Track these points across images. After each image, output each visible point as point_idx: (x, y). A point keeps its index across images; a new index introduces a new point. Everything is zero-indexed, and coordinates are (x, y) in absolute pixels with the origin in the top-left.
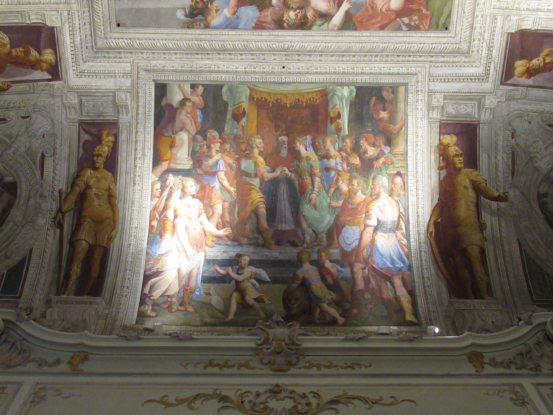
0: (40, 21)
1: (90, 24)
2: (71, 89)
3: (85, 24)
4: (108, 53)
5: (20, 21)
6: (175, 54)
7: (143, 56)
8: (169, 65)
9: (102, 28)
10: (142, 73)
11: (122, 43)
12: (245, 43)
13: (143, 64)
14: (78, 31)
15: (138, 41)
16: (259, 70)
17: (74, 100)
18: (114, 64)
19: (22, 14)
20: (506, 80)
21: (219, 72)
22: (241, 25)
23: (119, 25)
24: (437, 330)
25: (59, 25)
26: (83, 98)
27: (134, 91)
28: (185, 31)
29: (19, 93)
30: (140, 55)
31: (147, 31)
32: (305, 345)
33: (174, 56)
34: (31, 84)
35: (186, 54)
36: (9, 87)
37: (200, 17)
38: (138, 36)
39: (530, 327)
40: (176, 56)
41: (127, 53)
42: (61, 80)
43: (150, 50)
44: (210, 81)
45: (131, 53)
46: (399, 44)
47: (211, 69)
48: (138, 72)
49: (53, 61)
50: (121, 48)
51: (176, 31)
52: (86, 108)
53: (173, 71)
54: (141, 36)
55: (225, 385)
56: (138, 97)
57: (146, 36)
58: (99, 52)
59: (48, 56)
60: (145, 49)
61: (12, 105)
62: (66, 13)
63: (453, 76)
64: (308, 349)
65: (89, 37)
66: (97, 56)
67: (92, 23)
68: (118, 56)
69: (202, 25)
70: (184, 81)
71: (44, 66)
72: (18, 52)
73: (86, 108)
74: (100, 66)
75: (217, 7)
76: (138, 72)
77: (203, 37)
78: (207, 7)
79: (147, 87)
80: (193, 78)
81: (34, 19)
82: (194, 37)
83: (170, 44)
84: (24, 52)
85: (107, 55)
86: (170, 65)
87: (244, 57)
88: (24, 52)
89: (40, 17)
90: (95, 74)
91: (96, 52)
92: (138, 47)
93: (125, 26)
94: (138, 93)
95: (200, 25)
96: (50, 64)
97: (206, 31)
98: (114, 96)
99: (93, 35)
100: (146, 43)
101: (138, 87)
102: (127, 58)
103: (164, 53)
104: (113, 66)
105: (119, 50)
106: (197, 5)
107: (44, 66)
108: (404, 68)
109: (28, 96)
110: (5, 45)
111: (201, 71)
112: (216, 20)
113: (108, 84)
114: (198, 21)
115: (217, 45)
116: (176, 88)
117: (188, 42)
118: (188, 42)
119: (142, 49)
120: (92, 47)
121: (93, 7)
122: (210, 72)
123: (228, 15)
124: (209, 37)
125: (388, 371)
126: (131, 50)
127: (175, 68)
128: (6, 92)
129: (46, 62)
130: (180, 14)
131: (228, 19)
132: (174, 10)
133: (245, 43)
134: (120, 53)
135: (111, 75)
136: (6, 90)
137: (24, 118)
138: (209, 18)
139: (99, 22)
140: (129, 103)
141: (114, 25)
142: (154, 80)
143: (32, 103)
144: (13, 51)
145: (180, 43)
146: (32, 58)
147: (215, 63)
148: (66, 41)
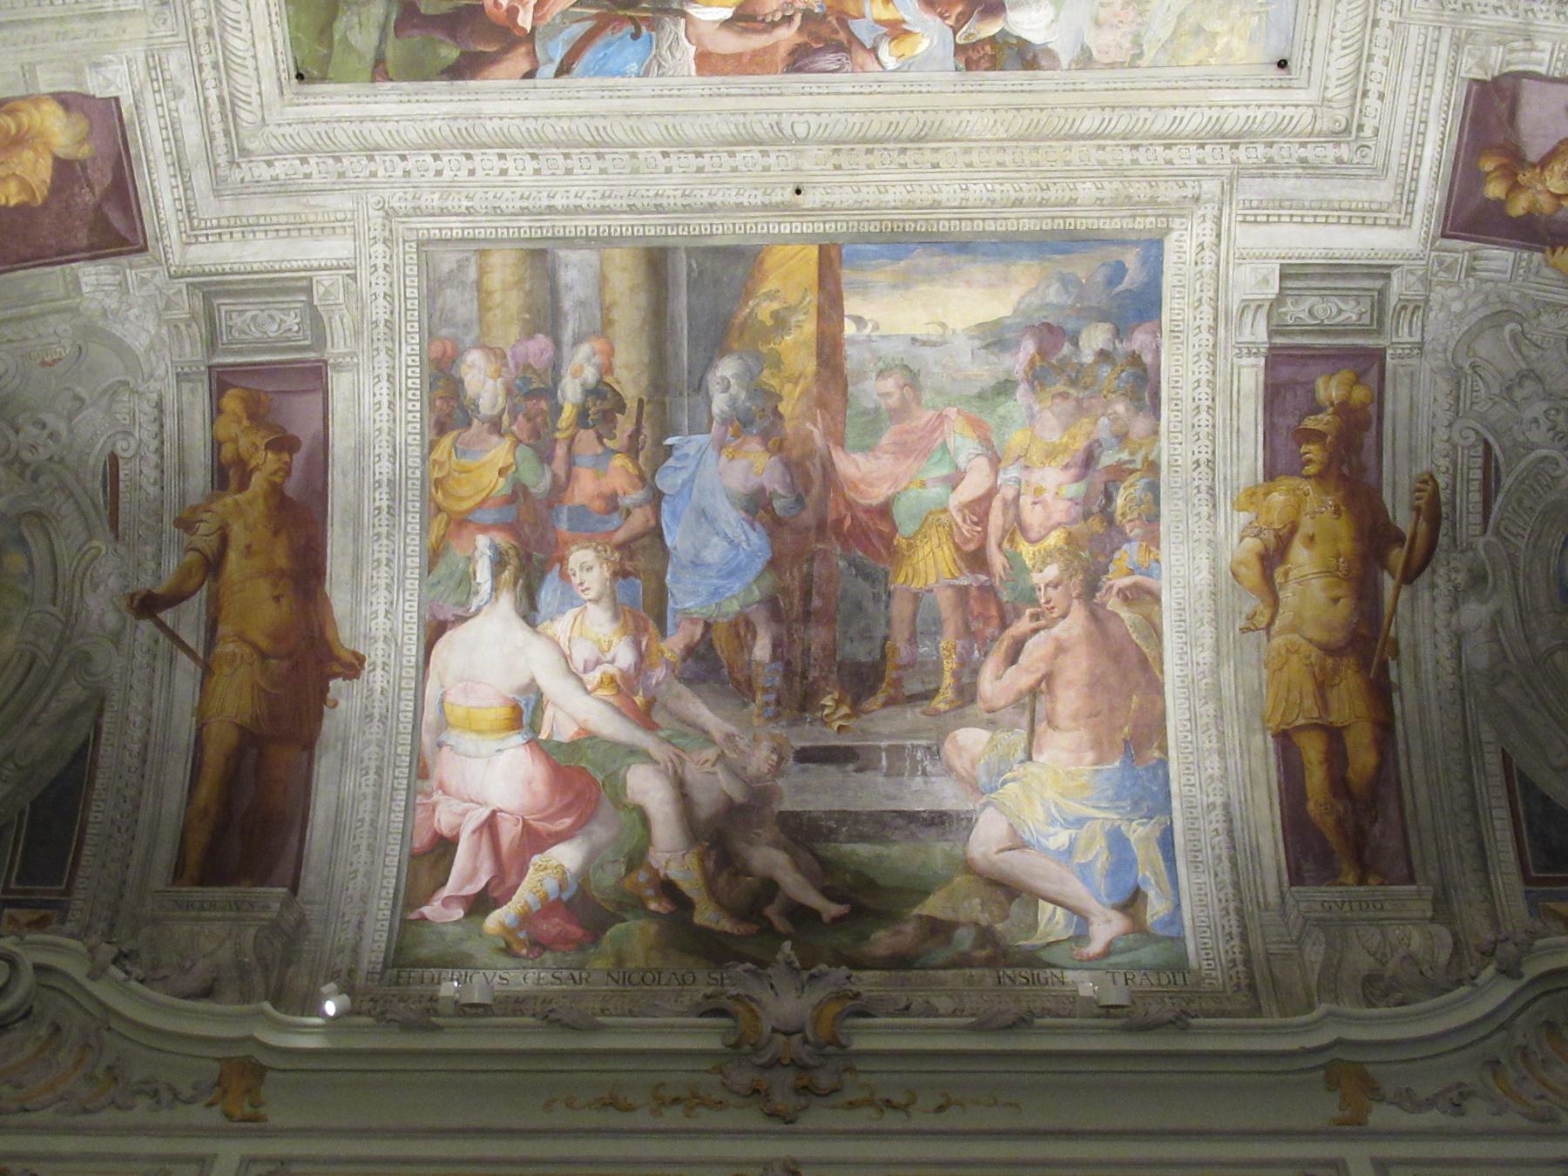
16: (565, 202)
20: (124, 241)
24: (330, 1008)
32: (860, 1043)
39: (1518, 984)
43: (591, 146)
46: (835, 116)
63: (1281, 207)
64: (861, 1054)
92: (588, 138)
93: (313, 80)
108: (1007, 186)
125: (1118, 1123)
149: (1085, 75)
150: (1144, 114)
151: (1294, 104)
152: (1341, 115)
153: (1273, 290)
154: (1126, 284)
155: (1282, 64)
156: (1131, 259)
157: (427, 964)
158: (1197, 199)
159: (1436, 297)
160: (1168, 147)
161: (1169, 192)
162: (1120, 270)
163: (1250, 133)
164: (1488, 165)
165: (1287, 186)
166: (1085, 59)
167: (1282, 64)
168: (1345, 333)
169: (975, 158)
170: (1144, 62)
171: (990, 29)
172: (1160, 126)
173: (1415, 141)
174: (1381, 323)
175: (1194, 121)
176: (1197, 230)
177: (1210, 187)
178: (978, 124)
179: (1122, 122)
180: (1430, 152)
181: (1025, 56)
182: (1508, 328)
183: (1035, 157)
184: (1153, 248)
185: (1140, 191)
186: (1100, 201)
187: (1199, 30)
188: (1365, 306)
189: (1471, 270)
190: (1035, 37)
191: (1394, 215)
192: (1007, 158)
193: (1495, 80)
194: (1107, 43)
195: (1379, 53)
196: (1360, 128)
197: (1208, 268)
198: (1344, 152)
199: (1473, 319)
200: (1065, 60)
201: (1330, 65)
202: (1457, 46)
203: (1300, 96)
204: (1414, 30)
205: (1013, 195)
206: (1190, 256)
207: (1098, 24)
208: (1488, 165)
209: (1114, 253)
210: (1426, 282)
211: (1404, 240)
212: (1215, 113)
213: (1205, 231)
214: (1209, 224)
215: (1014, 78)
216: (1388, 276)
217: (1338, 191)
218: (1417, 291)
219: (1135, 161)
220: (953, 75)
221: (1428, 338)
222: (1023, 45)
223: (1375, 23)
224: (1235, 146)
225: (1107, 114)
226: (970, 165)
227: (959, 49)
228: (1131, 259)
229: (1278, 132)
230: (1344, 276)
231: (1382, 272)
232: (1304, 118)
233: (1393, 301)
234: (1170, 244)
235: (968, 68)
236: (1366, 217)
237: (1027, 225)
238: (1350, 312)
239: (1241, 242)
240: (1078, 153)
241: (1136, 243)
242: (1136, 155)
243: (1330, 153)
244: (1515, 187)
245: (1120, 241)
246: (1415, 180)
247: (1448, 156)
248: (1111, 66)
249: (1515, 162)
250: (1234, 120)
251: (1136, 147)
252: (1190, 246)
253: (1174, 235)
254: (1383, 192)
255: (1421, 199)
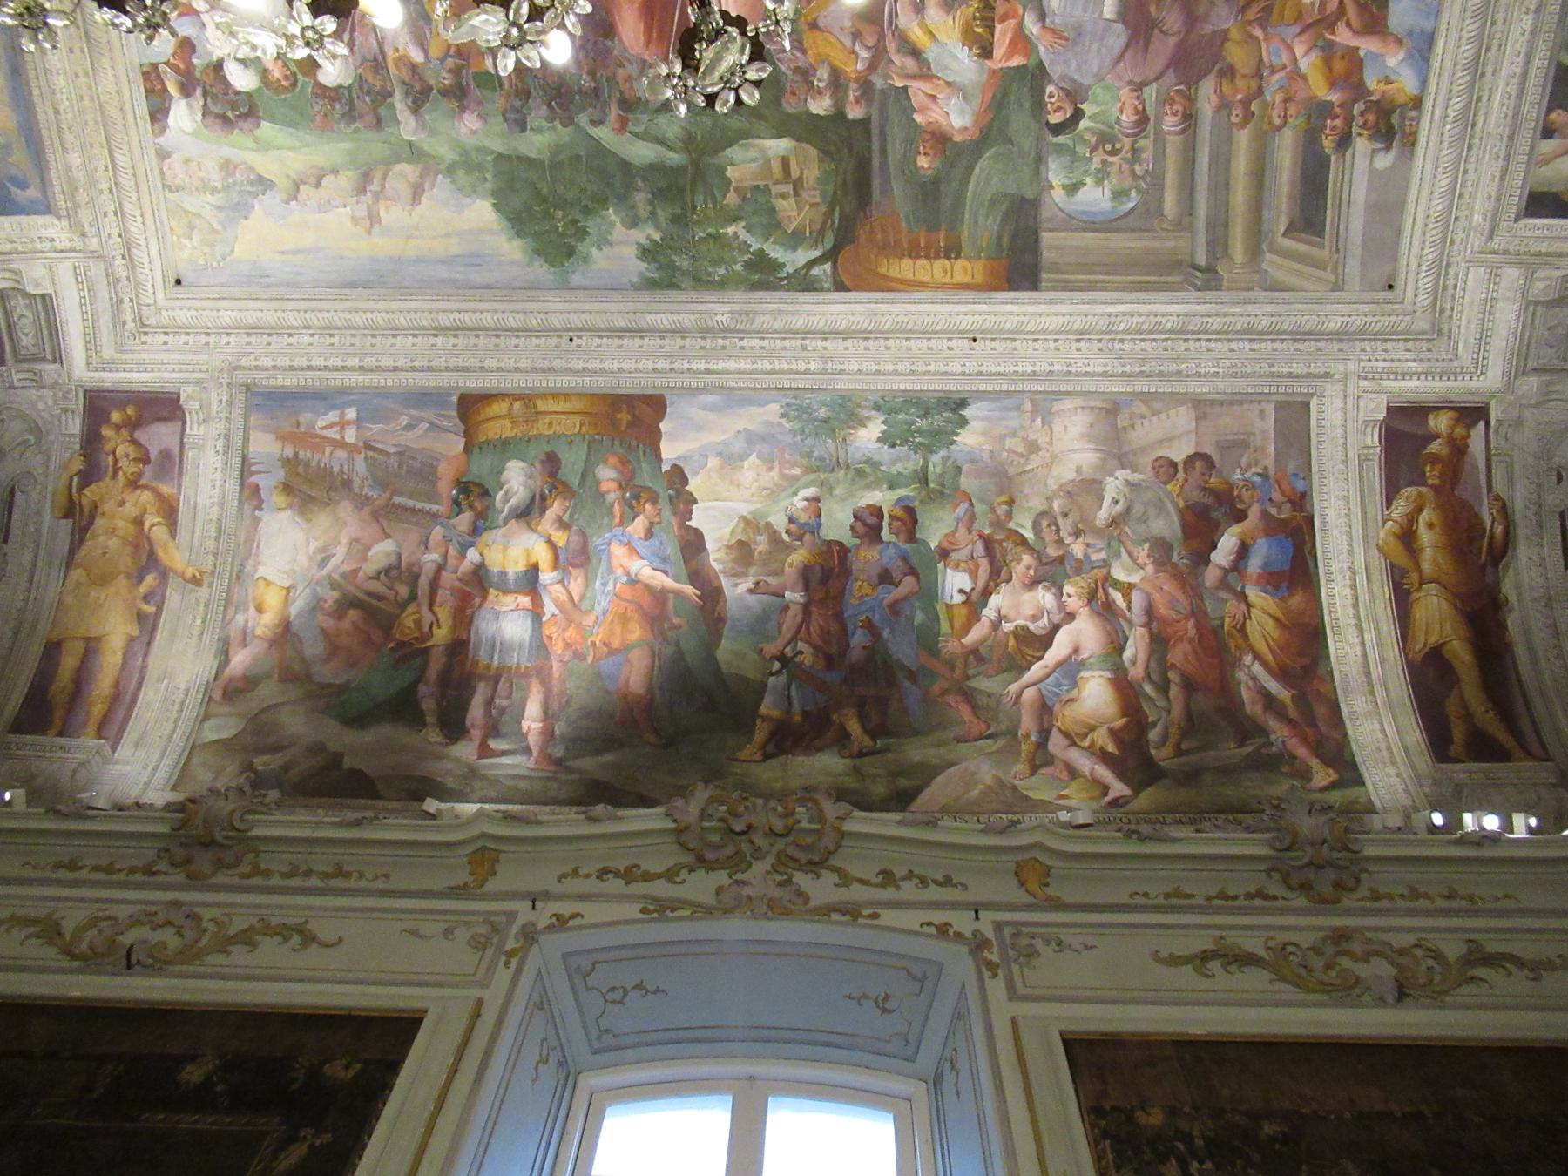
0: (1377, 430)
1: (1385, 341)
2: (1508, 388)
3: (1385, 350)
4: (1442, 311)
5: (1376, 464)
6: (1465, 172)
7: (1458, 241)
8: (1488, 187)
9: (1393, 318)
10: (1495, 244)
11: (1426, 282)
12: (1468, 14)
13: (1476, 242)
14: (1397, 364)
15: (1427, 251)
17: (1531, 384)
18: (1467, 299)
19: (1363, 459)
21: (1525, 75)
22: (1427, 25)
23: (1390, 287)
25: (1384, 397)
26: (1530, 365)
27: (1532, 262)
28: (1420, 151)
29: (1511, 481)
30: (1455, 247)
31: (1407, 234)
33: (1471, 176)
34: (1494, 459)
35: (1470, 148)
36: (1498, 498)
37: (1395, 120)
38: (1415, 251)
40: (1471, 171)
41: (1447, 274)
42: (1488, 404)
44: (1542, 96)
45: (1448, 265)
47: (1514, 94)
48: (1493, 252)
49: (1451, 414)
50: (1436, 285)
51: (1417, 170)
52: (1555, 362)
53: (1502, 179)
54: (1416, 243)
55: (320, 908)
56: (1547, 254)
57: (1418, 233)
58: (1438, 330)
59: (1440, 423)
60: (1445, 239)
61: (1534, 496)
62: (1363, 383)
65: (1410, 345)
66: (1446, 330)
67: (1385, 336)
68: (1450, 290)
69: (1413, 114)
70: (1530, 154)
71: (1459, 431)
72: (1432, 473)
73: (1555, 362)
74: (1467, 328)
75: (1379, 82)
76: (1493, 252)
77: (1438, 112)
78: (1377, 102)
79: (1529, 234)
80: (1526, 135)
81: (1373, 439)
82: (1434, 132)
83: (1443, 183)
84: (1433, 463)
85: (1448, 313)
86: (1489, 183)
87: (1500, 17)
88: (1433, 463)
89: (1369, 430)
90: (1483, 342)
91: (1440, 331)
94: (1539, 254)
95: (1412, 119)
96: (1457, 420)
97: (1428, 104)
98: (1537, 303)
99: (1407, 336)
100: (1433, 233)
101: (1525, 253)
102: (1457, 274)
103: (1461, 196)
104: (1472, 303)
105: (1439, 290)
106: (1370, 124)
107: (1459, 431)
109: (1516, 467)
110: (1420, 495)
111: (1516, 115)
112: (1407, 83)
113: (1507, 315)
114: (1402, 126)
115: (1463, 77)
116: (1545, 172)
117: (1445, 144)
118: (1445, 144)
119: (1444, 241)
120: (1429, 340)
121: (1355, 333)
122: (1520, 95)
123: (1401, 55)
124: (1440, 100)
126: (1442, 266)
127: (1498, 175)
128: (1509, 504)
129: (1452, 428)
130: (1384, 161)
131: (1410, 56)
132: (1372, 171)
133: (1468, 14)
134: (1445, 288)
135: (1487, 308)
136: (1504, 506)
137: (1560, 479)
138: (1401, 100)
139: (1382, 323)
140: (1559, 273)
141: (1389, 295)
142: (1517, 220)
143: (1530, 460)
144: (1430, 482)
145: (1445, 160)
146: (1445, 451)
147: (1501, 83)
148: (1413, 387)
149: (153, 155)
150: (134, 196)
151: (155, 291)
152: (152, 321)
153: (31, 290)
154: (13, 189)
155: (178, 282)
156: (32, 193)
157: (698, 575)
158: (84, 235)
159: (47, 393)
160: (116, 213)
161: (85, 217)
162: (23, 185)
163: (134, 267)
164: (130, 411)
165: (104, 294)
166: (163, 155)
167: (178, 282)
168: (11, 338)
169: (83, 79)
170: (168, 195)
171: (172, 89)
172: (127, 207)
173: (142, 367)
174: (24, 361)
175: (135, 229)
176: (63, 237)
177: (94, 243)
178: (107, 83)
179: (126, 182)
180: (135, 376)
181: (158, 114)
182: (31, 438)
183: (91, 123)
184: (47, 209)
185: (82, 197)
186: (69, 169)
187: (192, 228)
188: (33, 350)
189: (66, 411)
190: (171, 120)
191: (94, 361)
192: (87, 102)
193: (180, 407)
194: (175, 164)
195: (191, 338)
196: (146, 334)
197: (39, 246)
198: (130, 325)
199: (34, 416)
200: (160, 140)
201: (182, 310)
202: (198, 382)
203: (160, 295)
204: (205, 357)
205: (61, 108)
206: (43, 233)
207: (187, 161)
208: (130, 411)
209: (35, 180)
210: (55, 385)
211: (80, 367)
212: (142, 242)
213: (63, 241)
214: (69, 245)
215: (143, 108)
216: (54, 361)
217: (105, 323)
218: (47, 380)
219: (101, 192)
220: (137, 62)
221: (19, 391)
222: (166, 112)
223: (208, 334)
224: (124, 258)
225: (130, 171)
226: (77, 76)
227: (155, 66)
228: (32, 193)
229: (137, 283)
230: (50, 333)
231: (57, 358)
232: (147, 298)
233: (39, 367)
234: (49, 219)
235: (144, 73)
236: (91, 343)
237: (41, 117)
238: (27, 341)
239: (60, 266)
240: (102, 159)
241: (45, 196)
242: (106, 192)
243: (129, 317)
244: (118, 428)
245: (44, 184)
246: (118, 370)
247: (134, 387)
248: (162, 173)
249: (133, 425)
250: (140, 255)
251: (111, 191)
252: (50, 232)
253: (56, 221)
254: (108, 352)
255: (106, 375)
